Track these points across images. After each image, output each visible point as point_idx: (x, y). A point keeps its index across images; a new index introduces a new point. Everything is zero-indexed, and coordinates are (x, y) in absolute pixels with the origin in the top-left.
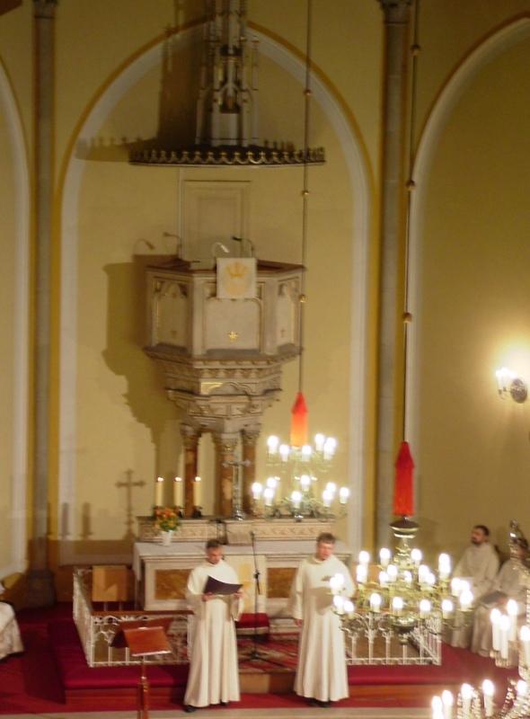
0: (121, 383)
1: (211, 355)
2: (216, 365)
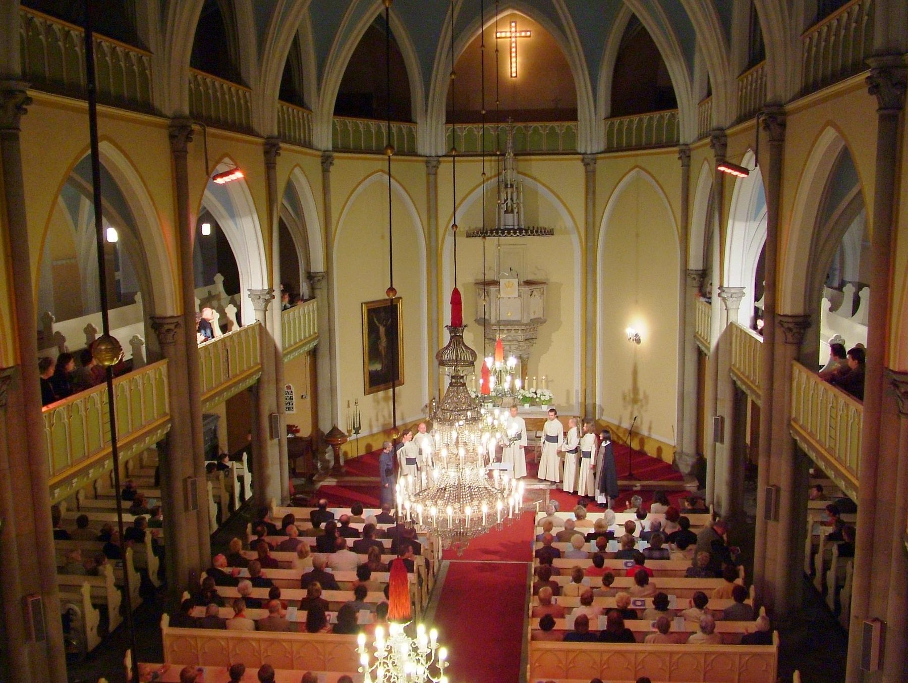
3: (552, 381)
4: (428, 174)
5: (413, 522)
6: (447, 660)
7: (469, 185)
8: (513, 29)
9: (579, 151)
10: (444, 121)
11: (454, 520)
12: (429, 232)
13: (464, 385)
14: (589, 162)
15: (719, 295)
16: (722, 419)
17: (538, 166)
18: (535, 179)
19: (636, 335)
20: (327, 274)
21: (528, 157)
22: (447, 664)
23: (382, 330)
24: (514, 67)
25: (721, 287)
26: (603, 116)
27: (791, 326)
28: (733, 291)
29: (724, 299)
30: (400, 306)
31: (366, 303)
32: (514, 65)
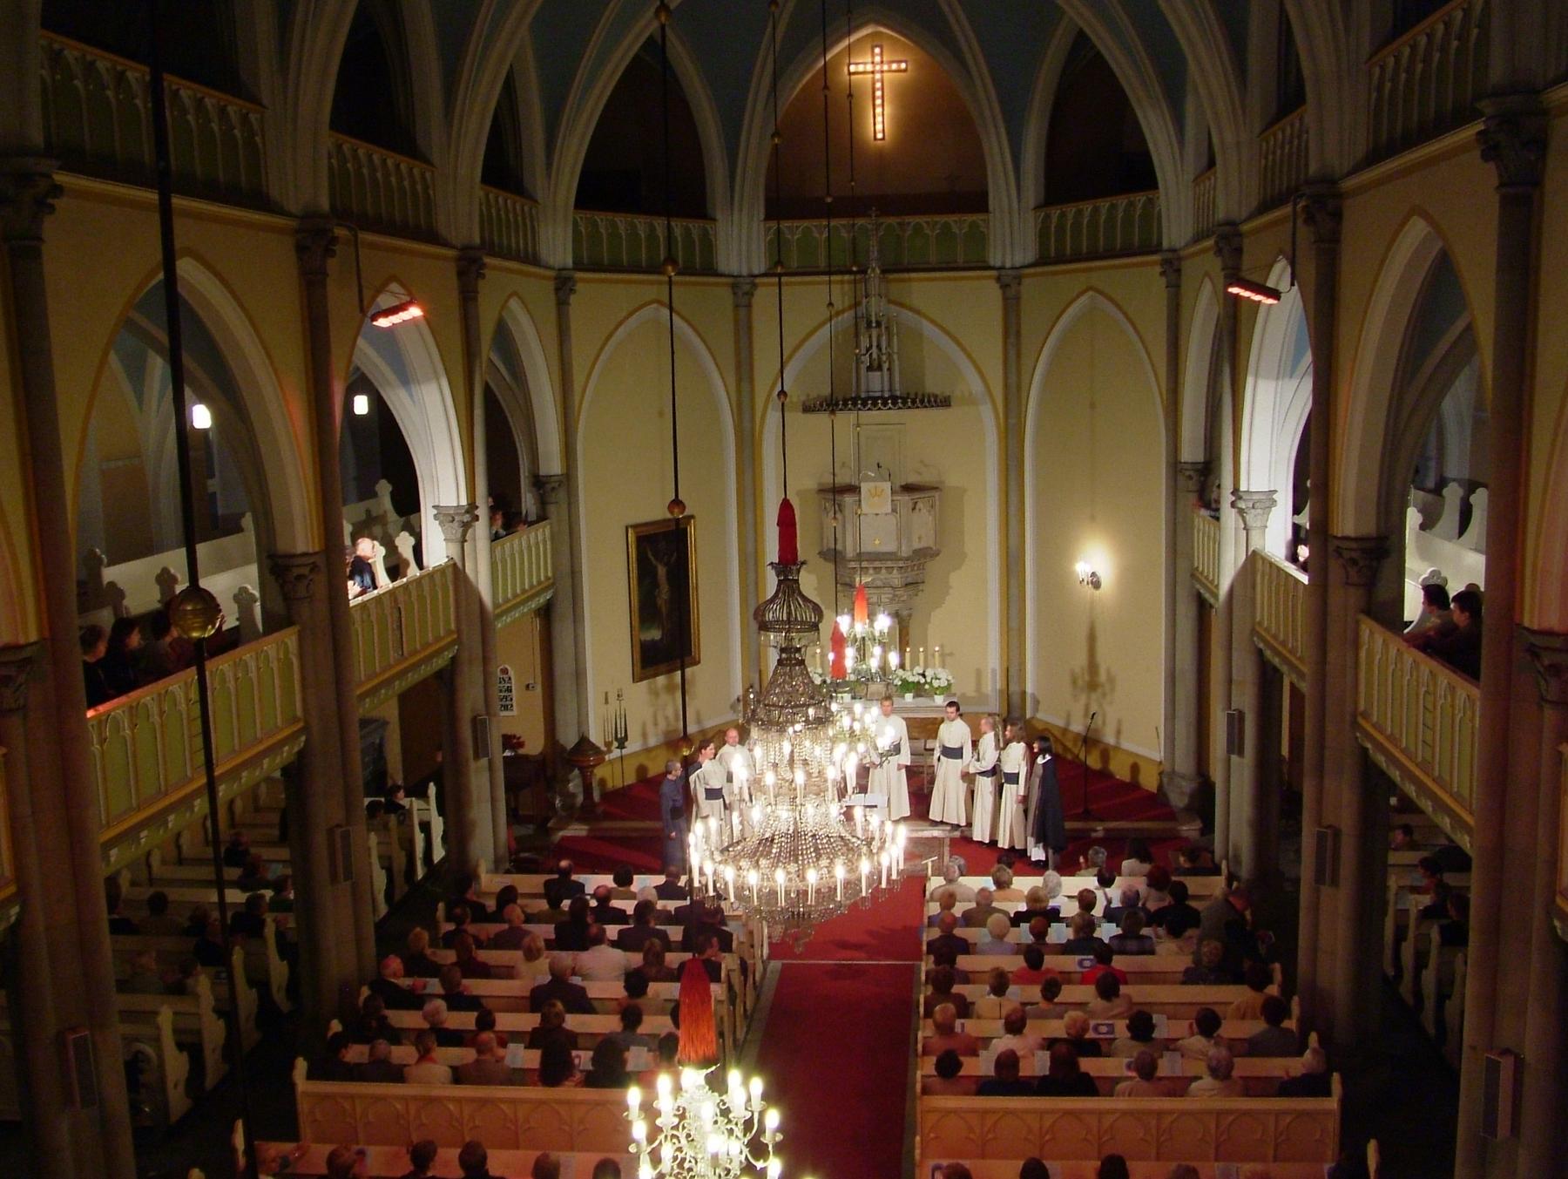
1: (860, 557)
3: (951, 654)
4: (737, 306)
6: (780, 1129)
7: (804, 324)
8: (878, 59)
9: (992, 263)
10: (762, 216)
12: (739, 405)
13: (802, 662)
14: (1010, 281)
15: (1233, 505)
16: (1241, 714)
17: (925, 291)
18: (918, 312)
19: (1093, 574)
20: (568, 478)
21: (906, 275)
22: (779, 1137)
23: (662, 571)
24: (879, 123)
25: (1236, 491)
26: (1032, 204)
27: (1354, 555)
28: (1255, 497)
29: (1241, 512)
30: (691, 530)
31: (635, 527)
32: (879, 119)
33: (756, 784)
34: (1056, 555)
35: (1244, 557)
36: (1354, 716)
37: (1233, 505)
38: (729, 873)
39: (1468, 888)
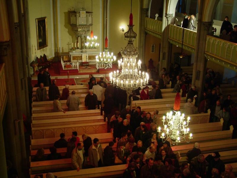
0: (67, 30)
1: (80, 25)
2: (80, 27)
3: (67, 44)
5: (115, 85)
6: (189, 120)
11: (133, 85)
13: (132, 44)
15: (165, 16)
19: (123, 29)
22: (190, 121)
23: (42, 28)
25: (166, 14)
27: (207, 25)
28: (170, 15)
29: (167, 18)
30: (46, 20)
31: (37, 19)
33: (126, 66)
34: (114, 26)
35: (167, 25)
36: (204, 52)
37: (165, 16)
38: (122, 82)
39: (192, 77)
